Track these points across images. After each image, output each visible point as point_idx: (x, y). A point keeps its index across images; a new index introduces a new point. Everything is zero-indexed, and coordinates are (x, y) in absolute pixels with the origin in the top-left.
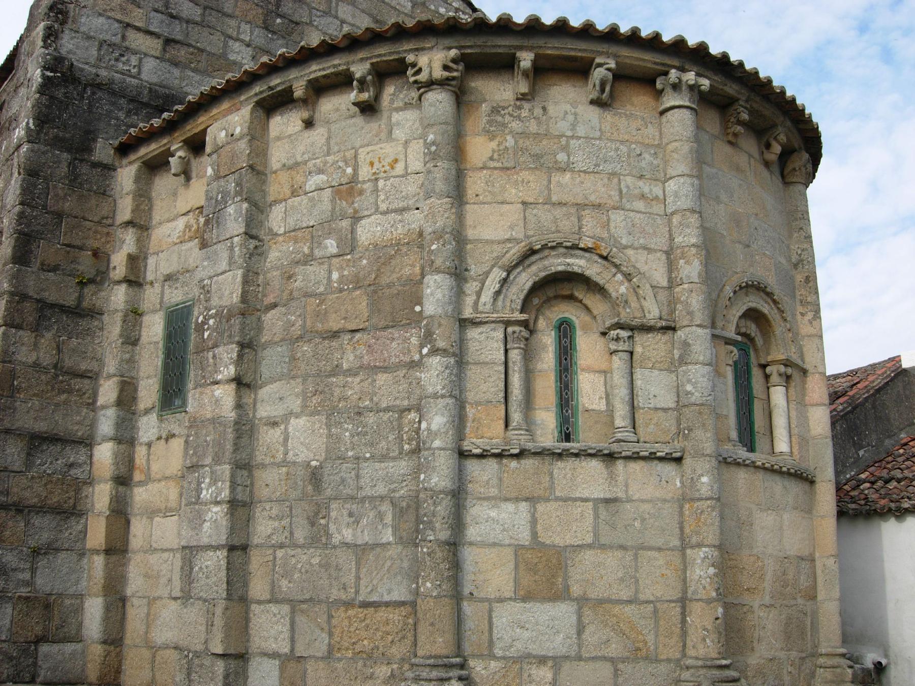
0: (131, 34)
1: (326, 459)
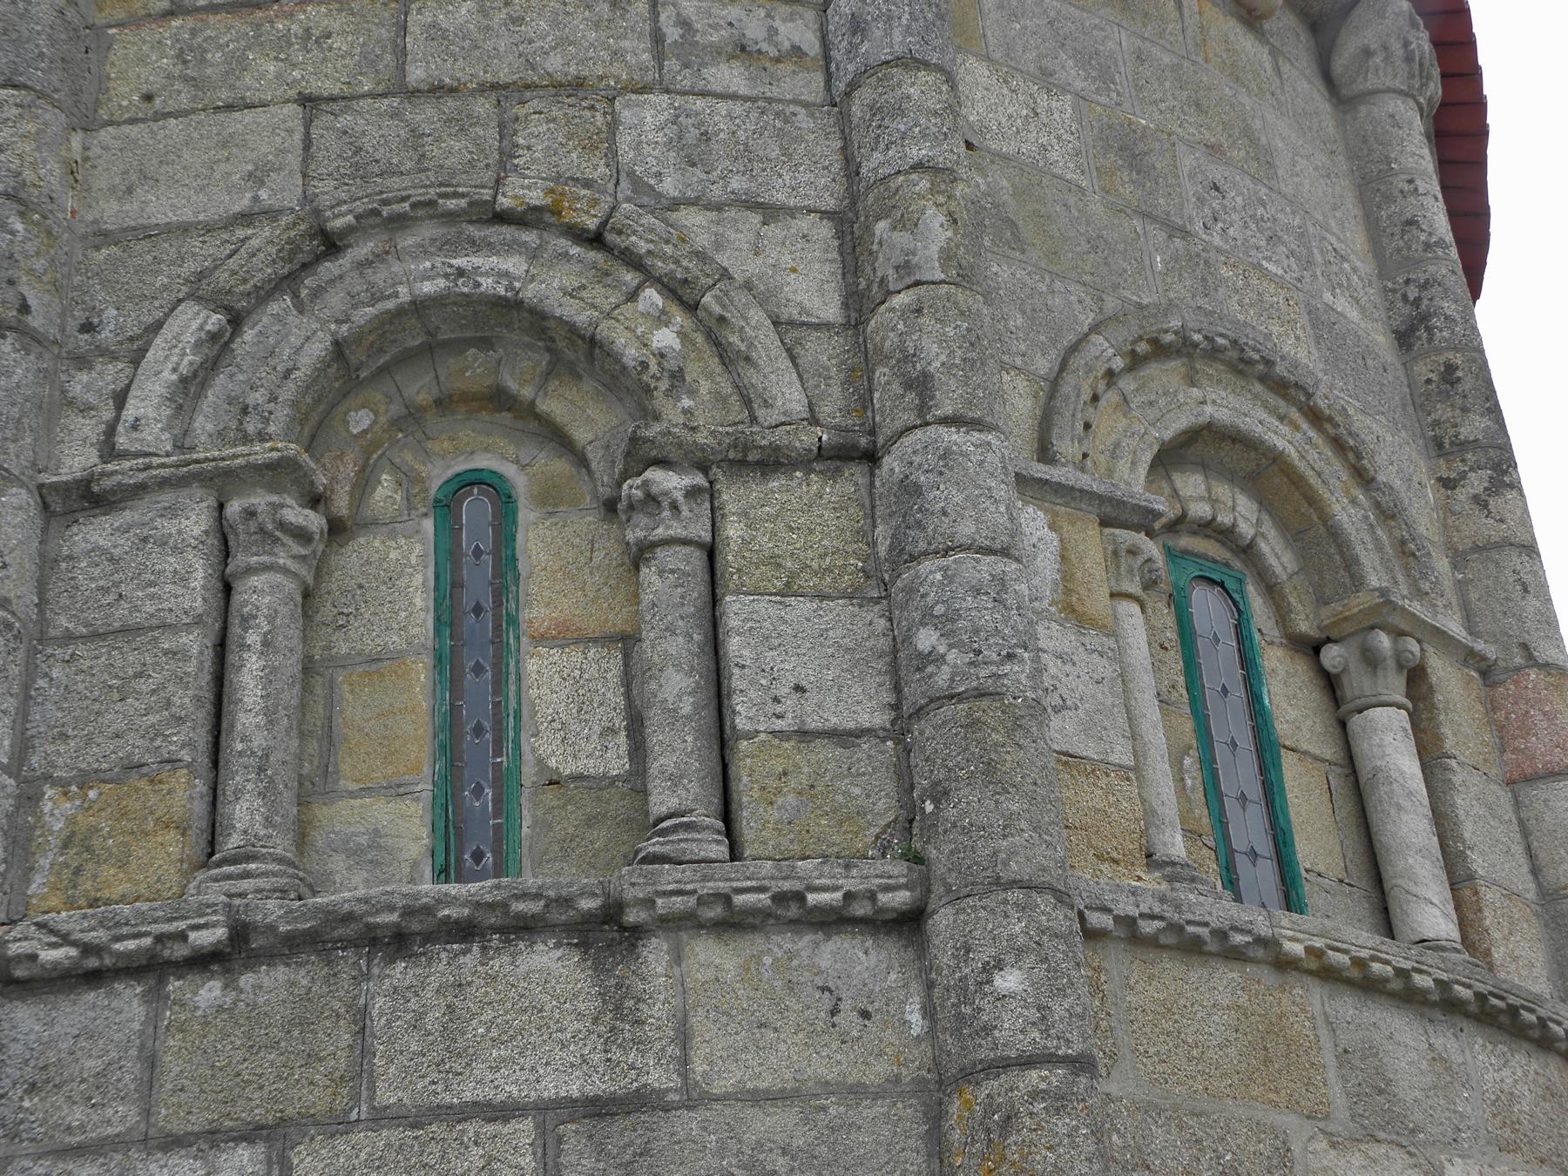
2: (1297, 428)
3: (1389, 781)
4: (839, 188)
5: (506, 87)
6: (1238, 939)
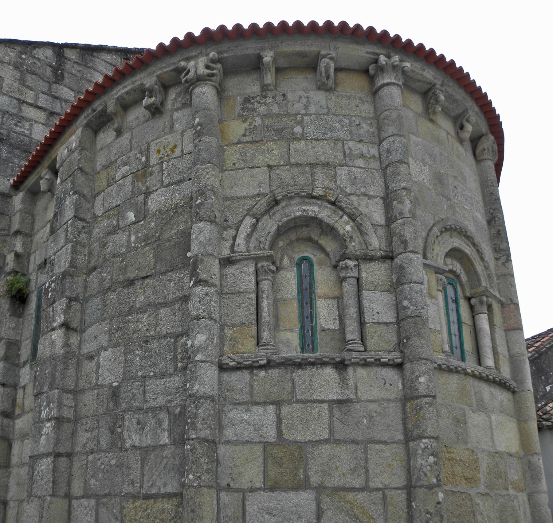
0: (25, 108)
1: (123, 380)
2: (470, 247)
3: (483, 331)
4: (384, 191)
5: (312, 164)
6: (460, 369)
